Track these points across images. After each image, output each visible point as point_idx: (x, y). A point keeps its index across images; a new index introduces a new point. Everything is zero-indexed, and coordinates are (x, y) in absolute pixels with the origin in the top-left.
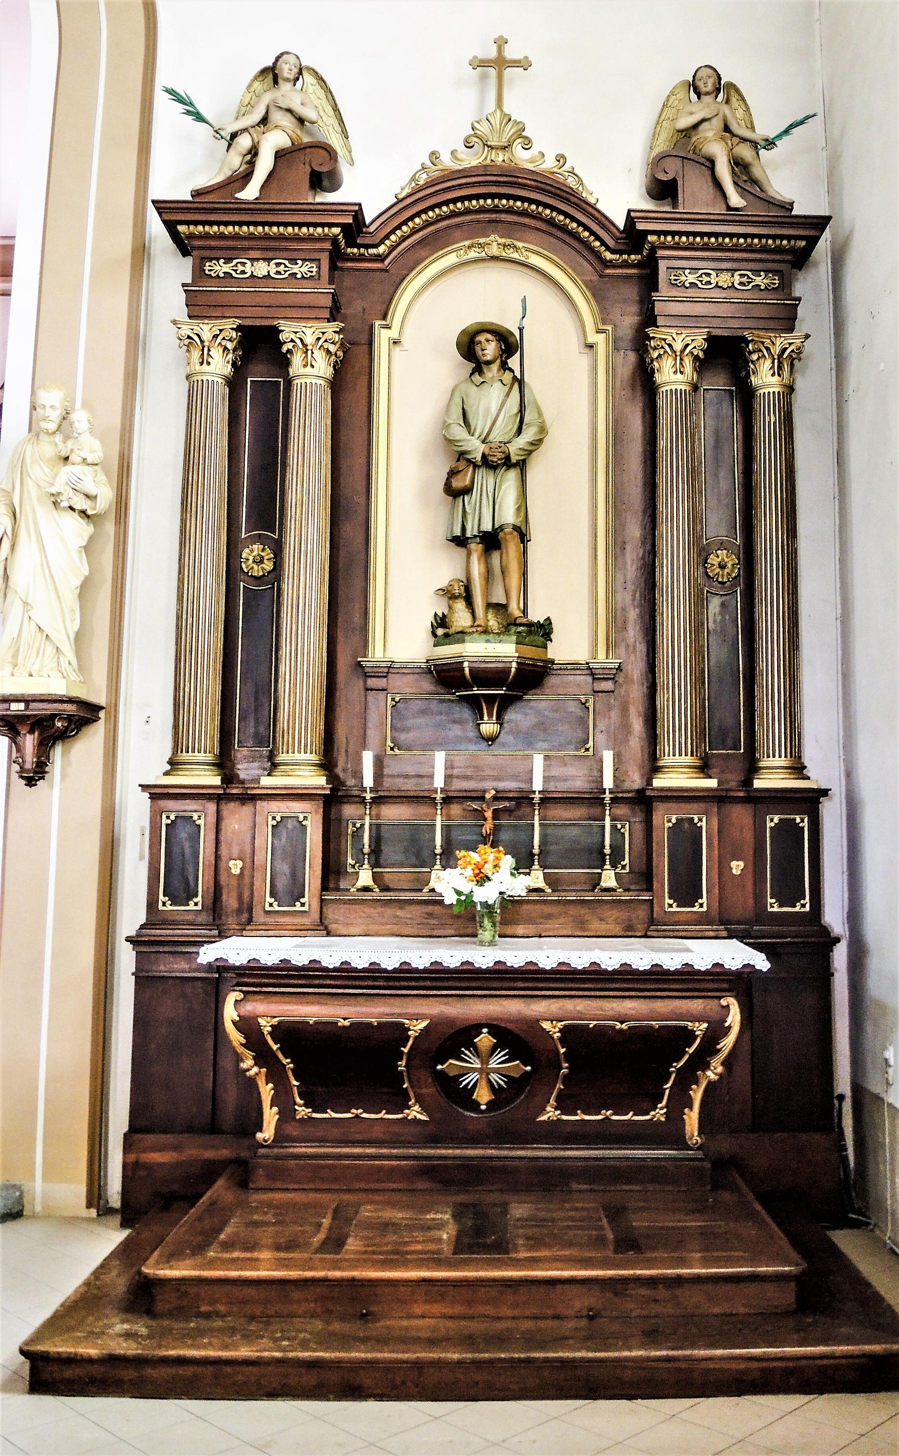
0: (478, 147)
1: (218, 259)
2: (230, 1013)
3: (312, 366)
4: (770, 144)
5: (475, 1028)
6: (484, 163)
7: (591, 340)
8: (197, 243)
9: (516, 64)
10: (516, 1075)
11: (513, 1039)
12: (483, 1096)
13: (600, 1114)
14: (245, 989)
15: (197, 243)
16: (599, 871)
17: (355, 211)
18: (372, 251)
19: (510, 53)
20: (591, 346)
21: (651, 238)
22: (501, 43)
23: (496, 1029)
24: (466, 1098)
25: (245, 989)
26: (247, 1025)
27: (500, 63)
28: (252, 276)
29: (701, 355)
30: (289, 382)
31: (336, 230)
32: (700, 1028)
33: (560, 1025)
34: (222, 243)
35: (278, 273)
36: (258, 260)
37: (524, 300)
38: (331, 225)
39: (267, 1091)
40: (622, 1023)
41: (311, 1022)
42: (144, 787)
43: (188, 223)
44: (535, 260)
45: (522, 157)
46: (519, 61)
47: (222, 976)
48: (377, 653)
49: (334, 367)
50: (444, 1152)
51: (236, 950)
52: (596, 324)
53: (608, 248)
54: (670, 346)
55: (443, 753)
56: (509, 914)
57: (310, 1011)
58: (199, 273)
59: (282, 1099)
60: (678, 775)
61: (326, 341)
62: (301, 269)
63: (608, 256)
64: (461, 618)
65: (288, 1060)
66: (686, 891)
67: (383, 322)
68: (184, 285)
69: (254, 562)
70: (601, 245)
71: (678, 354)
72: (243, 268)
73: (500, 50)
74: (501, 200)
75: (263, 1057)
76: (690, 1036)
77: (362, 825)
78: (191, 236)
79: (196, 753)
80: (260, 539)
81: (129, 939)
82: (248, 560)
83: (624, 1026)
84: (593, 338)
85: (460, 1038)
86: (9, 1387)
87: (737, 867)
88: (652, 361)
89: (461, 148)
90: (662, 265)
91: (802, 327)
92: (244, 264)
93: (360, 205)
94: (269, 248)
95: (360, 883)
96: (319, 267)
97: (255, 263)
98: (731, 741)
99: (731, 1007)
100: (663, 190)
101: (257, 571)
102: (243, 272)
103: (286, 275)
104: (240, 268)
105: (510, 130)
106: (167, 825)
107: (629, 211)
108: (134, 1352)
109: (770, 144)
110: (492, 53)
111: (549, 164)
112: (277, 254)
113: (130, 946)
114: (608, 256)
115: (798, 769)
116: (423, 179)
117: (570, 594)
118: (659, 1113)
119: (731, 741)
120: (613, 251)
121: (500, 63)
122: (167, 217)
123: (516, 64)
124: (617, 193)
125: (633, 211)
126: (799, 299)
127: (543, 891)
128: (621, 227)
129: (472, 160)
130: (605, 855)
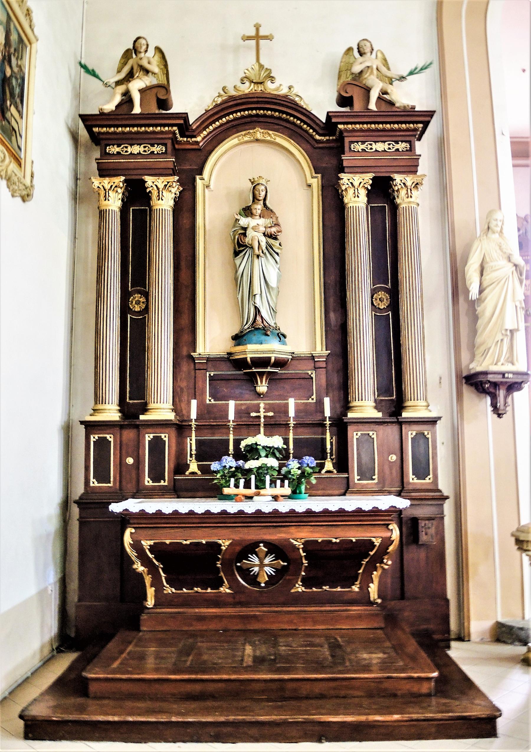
0: (247, 84)
1: (113, 145)
2: (127, 539)
3: (162, 200)
5: (256, 544)
6: (251, 92)
7: (309, 182)
8: (104, 137)
9: (266, 38)
10: (279, 567)
11: (277, 550)
12: (263, 579)
13: (192, 589)
14: (135, 526)
15: (104, 137)
16: (323, 461)
17: (185, 117)
18: (193, 139)
19: (262, 33)
20: (309, 186)
21: (341, 126)
22: (257, 27)
23: (267, 544)
24: (253, 580)
25: (135, 526)
26: (137, 546)
27: (257, 37)
28: (376, 151)
29: (369, 188)
30: (151, 210)
31: (175, 128)
32: (377, 542)
33: (303, 541)
34: (115, 136)
35: (389, 149)
36: (378, 142)
38: (172, 125)
39: (148, 580)
40: (336, 539)
41: (319, 541)
42: (82, 423)
43: (343, 123)
44: (279, 140)
45: (270, 87)
46: (267, 36)
47: (125, 520)
49: (174, 200)
50: (164, 610)
51: (133, 505)
52: (311, 174)
53: (318, 133)
54: (351, 183)
55: (293, 399)
57: (319, 536)
58: (105, 154)
59: (157, 583)
61: (170, 186)
62: (156, 149)
63: (318, 137)
65: (307, 562)
67: (200, 176)
68: (96, 159)
69: (136, 303)
70: (314, 132)
71: (107, 190)
72: (371, 147)
73: (257, 30)
75: (146, 561)
76: (372, 545)
78: (100, 133)
79: (360, 401)
80: (139, 292)
81: (75, 502)
82: (132, 302)
83: (338, 541)
84: (310, 181)
85: (250, 548)
86: (11, 734)
87: (130, 461)
88: (342, 191)
89: (239, 84)
90: (347, 140)
91: (421, 170)
92: (127, 147)
93: (187, 113)
95: (191, 470)
96: (166, 148)
97: (377, 144)
99: (394, 531)
100: (344, 101)
101: (137, 309)
102: (371, 149)
103: (149, 152)
104: (125, 149)
105: (263, 74)
106: (412, 438)
107: (328, 113)
110: (253, 33)
111: (284, 91)
112: (124, 142)
113: (76, 505)
114: (318, 137)
116: (219, 100)
118: (355, 588)
120: (320, 135)
121: (257, 37)
122: (89, 123)
123: (266, 38)
124: (321, 102)
125: (330, 112)
126: (420, 156)
127: (196, 473)
128: (324, 121)
129: (247, 88)
130: (290, 454)
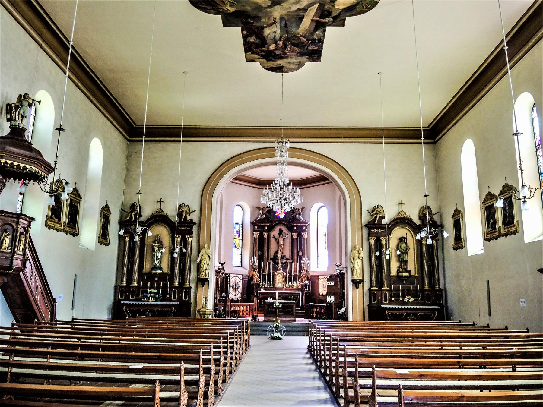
4: (434, 215)
27: (402, 204)
37: (488, 282)
48: (391, 274)
56: (412, 303)
60: (374, 288)
64: (401, 270)
66: (428, 301)
74: (402, 221)
77: (290, 299)
94: (378, 228)
98: (432, 283)
108: (308, 382)
109: (434, 215)
115: (439, 287)
117: (412, 267)
119: (432, 283)
